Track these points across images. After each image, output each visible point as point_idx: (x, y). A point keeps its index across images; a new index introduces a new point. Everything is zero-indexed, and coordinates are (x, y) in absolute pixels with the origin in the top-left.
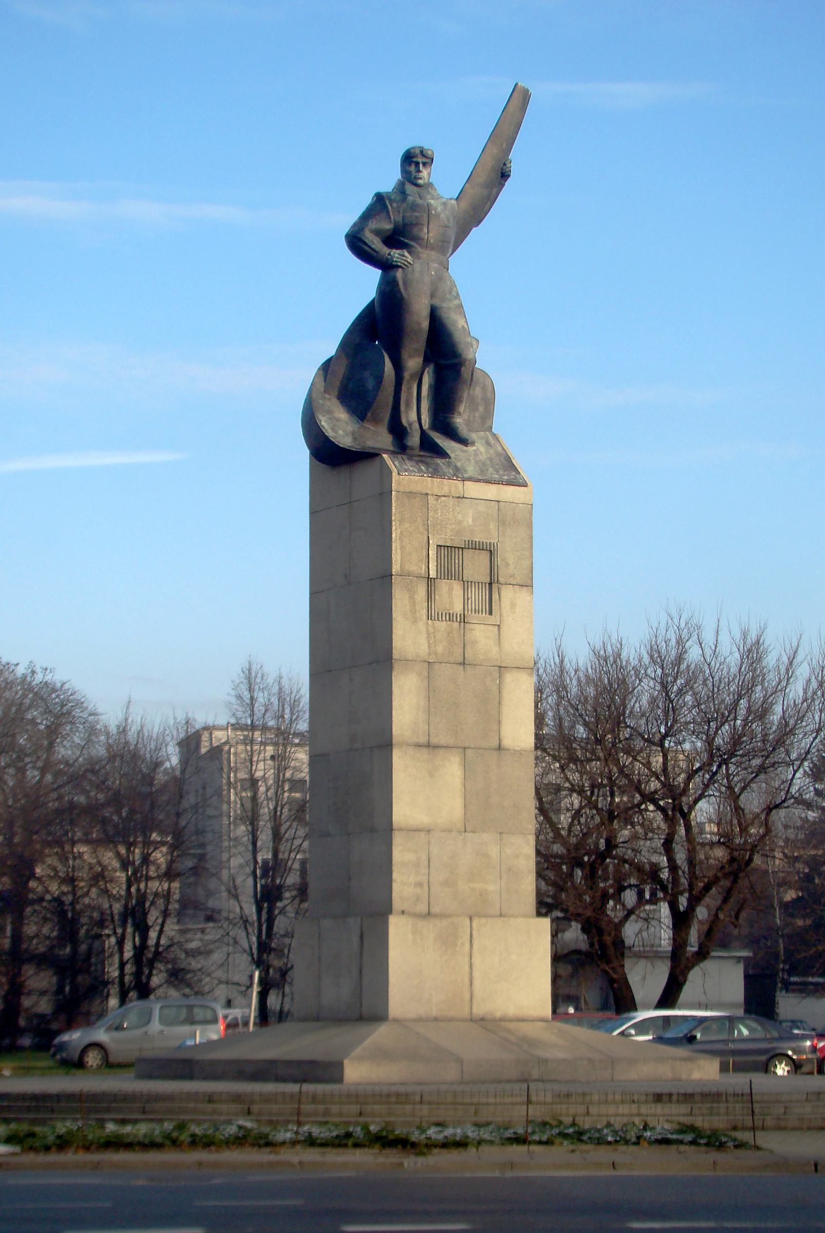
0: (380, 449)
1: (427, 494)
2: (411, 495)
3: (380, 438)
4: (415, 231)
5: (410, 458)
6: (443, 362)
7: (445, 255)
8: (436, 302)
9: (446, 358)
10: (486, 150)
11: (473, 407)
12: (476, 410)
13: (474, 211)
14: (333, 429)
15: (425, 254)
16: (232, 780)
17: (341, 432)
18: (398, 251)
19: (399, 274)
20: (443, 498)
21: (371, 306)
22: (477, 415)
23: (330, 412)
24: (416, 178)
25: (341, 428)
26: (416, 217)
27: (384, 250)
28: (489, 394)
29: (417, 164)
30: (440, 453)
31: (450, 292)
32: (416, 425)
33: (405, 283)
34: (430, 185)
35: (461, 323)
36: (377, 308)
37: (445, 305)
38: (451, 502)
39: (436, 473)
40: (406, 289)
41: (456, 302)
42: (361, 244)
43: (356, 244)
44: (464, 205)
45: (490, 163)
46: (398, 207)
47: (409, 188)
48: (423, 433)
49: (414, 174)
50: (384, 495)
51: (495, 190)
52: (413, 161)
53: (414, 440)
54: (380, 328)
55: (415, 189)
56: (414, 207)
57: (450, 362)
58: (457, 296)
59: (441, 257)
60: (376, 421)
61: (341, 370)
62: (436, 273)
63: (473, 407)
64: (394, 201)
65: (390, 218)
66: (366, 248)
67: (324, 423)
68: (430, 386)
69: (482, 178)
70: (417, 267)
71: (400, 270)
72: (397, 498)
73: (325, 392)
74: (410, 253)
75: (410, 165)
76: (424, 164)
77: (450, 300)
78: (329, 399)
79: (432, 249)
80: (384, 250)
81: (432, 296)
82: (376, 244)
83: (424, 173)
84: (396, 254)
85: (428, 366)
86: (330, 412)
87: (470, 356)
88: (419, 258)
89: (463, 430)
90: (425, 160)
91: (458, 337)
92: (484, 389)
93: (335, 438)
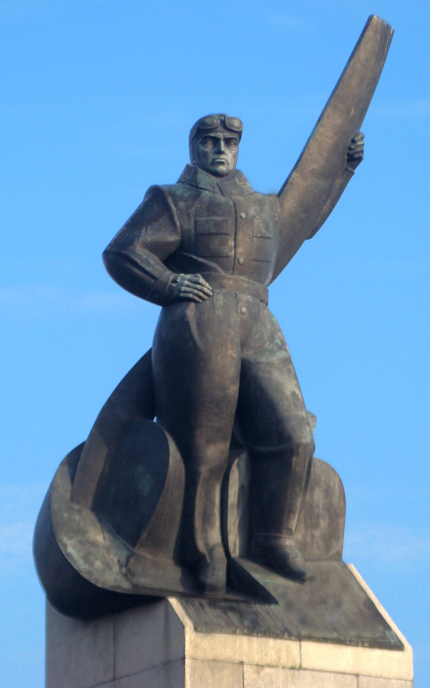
0: (161, 590)
1: (242, 663)
2: (215, 664)
3: (161, 571)
4: (215, 244)
5: (213, 603)
6: (262, 449)
7: (262, 282)
8: (249, 354)
9: (267, 443)
10: (325, 119)
11: (311, 522)
12: (316, 526)
13: (309, 211)
14: (86, 559)
15: (230, 280)
16: (278, 206)
17: (98, 564)
18: (188, 276)
19: (191, 311)
20: (267, 670)
21: (145, 361)
22: (317, 533)
23: (80, 532)
24: (215, 163)
25: (99, 557)
26: (217, 224)
27: (167, 275)
28: (335, 500)
29: (216, 141)
30: (263, 596)
31: (272, 338)
32: (220, 551)
33: (199, 325)
34: (236, 173)
35: (289, 387)
36: (156, 368)
37: (263, 359)
38: (281, 674)
39: (255, 628)
40: (202, 334)
41: (281, 354)
42: (129, 266)
43: (121, 264)
44: (290, 203)
45: (328, 138)
46: (188, 208)
47: (204, 179)
48: (232, 566)
49: (211, 157)
50: (173, 665)
51: (338, 182)
52: (210, 136)
53: (218, 575)
54: (158, 398)
55: (215, 180)
56: (212, 207)
57: (274, 449)
58: (282, 347)
59: (257, 284)
60: (156, 544)
61: (98, 465)
62: (248, 308)
63: (311, 522)
64: (181, 198)
65: (174, 224)
66: (137, 271)
67: (71, 548)
68: (241, 488)
69: (316, 162)
70: (220, 300)
71: (192, 305)
72: (194, 670)
73: (73, 499)
74: (207, 278)
75: (204, 143)
76: (228, 141)
77: (272, 352)
78: (79, 512)
79: (242, 273)
80: (167, 275)
81: (244, 345)
82: (154, 265)
83: (228, 155)
84: (185, 280)
85: (238, 456)
86: (80, 532)
87: (306, 440)
88: (222, 286)
89: (298, 560)
90: (228, 135)
91: (285, 407)
92: (328, 492)
93: (90, 573)
